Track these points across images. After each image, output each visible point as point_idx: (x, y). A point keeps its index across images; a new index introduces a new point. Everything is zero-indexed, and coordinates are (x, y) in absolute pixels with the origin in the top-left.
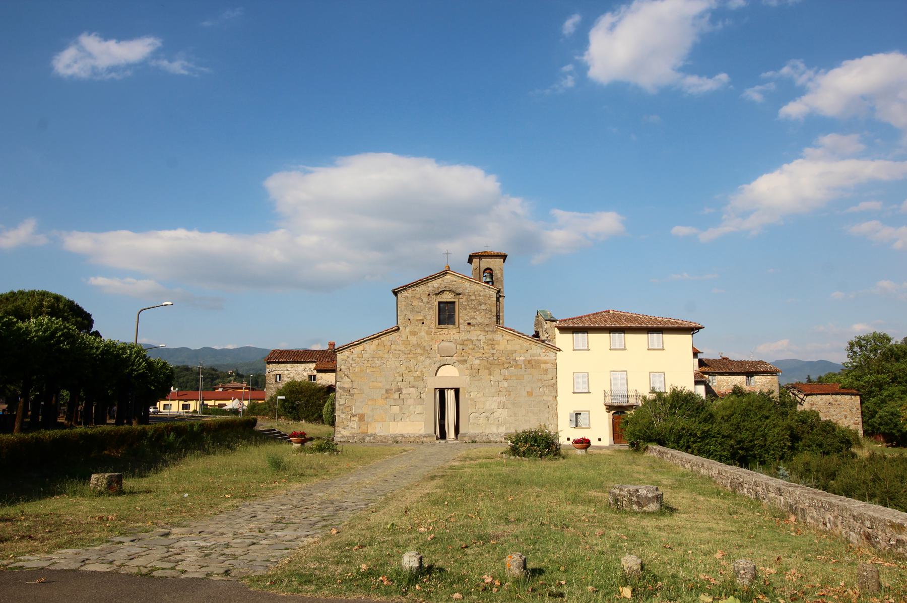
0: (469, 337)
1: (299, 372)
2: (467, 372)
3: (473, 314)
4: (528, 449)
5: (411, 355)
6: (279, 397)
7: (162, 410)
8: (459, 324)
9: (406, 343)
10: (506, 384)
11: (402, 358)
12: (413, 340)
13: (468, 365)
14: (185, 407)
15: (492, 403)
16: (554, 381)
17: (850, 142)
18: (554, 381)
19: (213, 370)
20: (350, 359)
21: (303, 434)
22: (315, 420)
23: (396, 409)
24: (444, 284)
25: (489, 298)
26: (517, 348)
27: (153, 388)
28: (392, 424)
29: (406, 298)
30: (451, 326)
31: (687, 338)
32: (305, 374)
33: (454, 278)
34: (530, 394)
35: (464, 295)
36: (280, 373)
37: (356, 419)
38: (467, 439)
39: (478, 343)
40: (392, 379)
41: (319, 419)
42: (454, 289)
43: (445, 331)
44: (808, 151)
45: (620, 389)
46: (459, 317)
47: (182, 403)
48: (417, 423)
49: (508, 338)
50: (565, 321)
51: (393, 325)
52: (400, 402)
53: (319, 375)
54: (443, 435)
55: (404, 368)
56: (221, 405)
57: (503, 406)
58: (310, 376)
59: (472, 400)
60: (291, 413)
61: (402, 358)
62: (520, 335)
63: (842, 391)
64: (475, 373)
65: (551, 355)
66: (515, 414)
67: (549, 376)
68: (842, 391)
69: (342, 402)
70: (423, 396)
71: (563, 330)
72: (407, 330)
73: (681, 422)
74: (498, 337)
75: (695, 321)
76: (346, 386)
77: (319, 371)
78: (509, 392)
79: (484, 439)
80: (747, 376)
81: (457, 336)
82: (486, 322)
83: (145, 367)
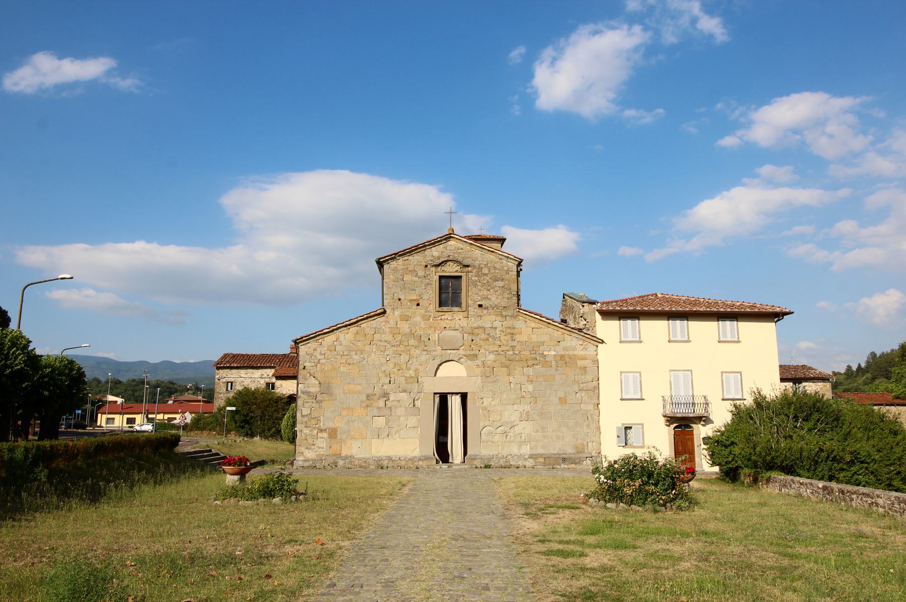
0: (480, 323)
1: (254, 379)
2: (478, 371)
3: (485, 293)
4: (639, 490)
5: (402, 348)
6: (229, 408)
7: (104, 424)
8: (467, 306)
9: (395, 331)
10: (530, 388)
11: (390, 351)
12: (405, 327)
13: (479, 362)
14: (131, 421)
15: (511, 414)
16: (595, 383)
17: (783, 173)
18: (595, 383)
19: (172, 383)
20: (317, 353)
21: (243, 460)
22: (272, 436)
23: (380, 422)
24: (447, 253)
25: (508, 272)
26: (545, 338)
27: (46, 393)
28: (375, 442)
29: (395, 270)
30: (456, 309)
31: (768, 328)
32: (262, 382)
33: (460, 245)
34: (563, 401)
35: (474, 267)
36: (232, 380)
37: (325, 435)
38: (477, 463)
39: (492, 333)
40: (375, 380)
41: (277, 435)
42: (460, 259)
43: (448, 316)
44: (745, 180)
45: (682, 394)
46: (467, 296)
47: (126, 416)
48: (412, 441)
49: (533, 325)
50: (608, 303)
51: (377, 307)
52: (387, 412)
53: (278, 383)
54: (443, 453)
55: (392, 365)
56: (170, 419)
57: (527, 417)
58: (268, 384)
59: (485, 409)
60: (243, 427)
61: (390, 351)
62: (549, 322)
63: (897, 401)
64: (488, 373)
65: (591, 348)
66: (543, 428)
67: (589, 377)
68: (897, 401)
69: (306, 411)
70: (418, 403)
71: (607, 314)
72: (397, 313)
73: (808, 441)
74: (519, 323)
75: (779, 305)
76: (312, 390)
77: (279, 378)
78: (535, 398)
79: (502, 462)
80: (795, 383)
81: (464, 322)
82: (503, 304)
83: (25, 362)
